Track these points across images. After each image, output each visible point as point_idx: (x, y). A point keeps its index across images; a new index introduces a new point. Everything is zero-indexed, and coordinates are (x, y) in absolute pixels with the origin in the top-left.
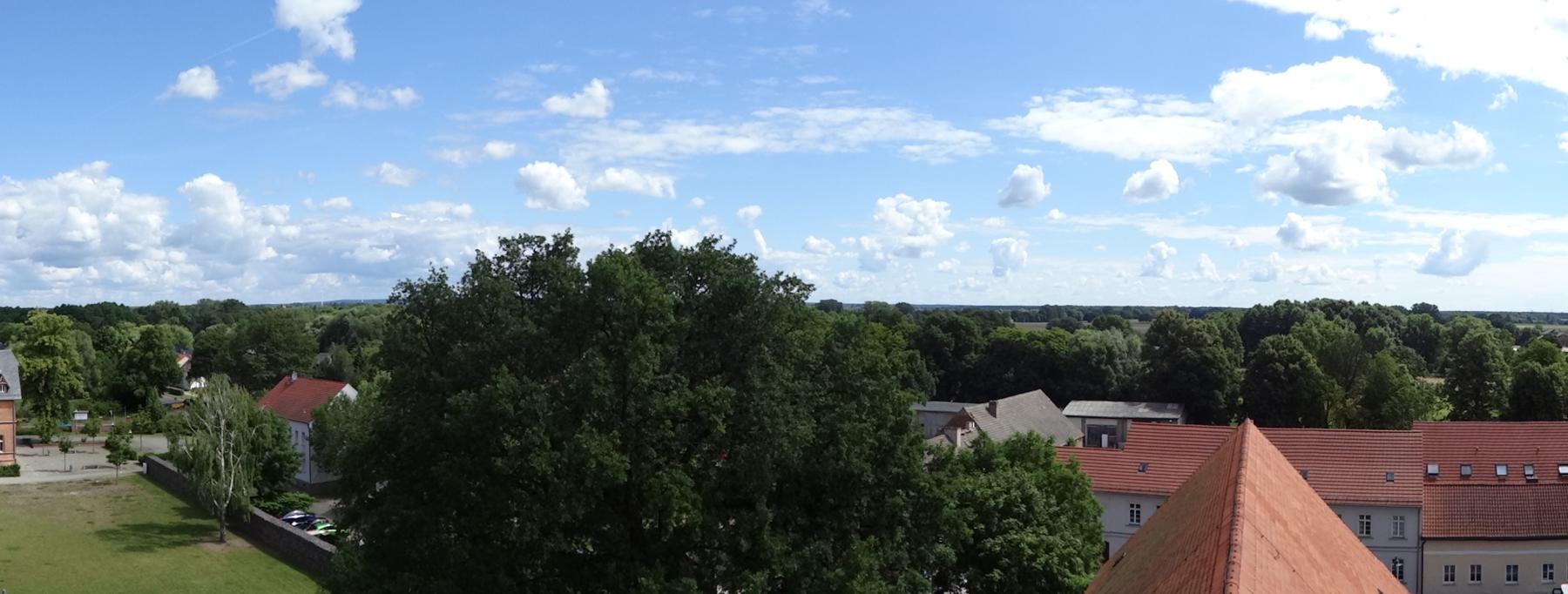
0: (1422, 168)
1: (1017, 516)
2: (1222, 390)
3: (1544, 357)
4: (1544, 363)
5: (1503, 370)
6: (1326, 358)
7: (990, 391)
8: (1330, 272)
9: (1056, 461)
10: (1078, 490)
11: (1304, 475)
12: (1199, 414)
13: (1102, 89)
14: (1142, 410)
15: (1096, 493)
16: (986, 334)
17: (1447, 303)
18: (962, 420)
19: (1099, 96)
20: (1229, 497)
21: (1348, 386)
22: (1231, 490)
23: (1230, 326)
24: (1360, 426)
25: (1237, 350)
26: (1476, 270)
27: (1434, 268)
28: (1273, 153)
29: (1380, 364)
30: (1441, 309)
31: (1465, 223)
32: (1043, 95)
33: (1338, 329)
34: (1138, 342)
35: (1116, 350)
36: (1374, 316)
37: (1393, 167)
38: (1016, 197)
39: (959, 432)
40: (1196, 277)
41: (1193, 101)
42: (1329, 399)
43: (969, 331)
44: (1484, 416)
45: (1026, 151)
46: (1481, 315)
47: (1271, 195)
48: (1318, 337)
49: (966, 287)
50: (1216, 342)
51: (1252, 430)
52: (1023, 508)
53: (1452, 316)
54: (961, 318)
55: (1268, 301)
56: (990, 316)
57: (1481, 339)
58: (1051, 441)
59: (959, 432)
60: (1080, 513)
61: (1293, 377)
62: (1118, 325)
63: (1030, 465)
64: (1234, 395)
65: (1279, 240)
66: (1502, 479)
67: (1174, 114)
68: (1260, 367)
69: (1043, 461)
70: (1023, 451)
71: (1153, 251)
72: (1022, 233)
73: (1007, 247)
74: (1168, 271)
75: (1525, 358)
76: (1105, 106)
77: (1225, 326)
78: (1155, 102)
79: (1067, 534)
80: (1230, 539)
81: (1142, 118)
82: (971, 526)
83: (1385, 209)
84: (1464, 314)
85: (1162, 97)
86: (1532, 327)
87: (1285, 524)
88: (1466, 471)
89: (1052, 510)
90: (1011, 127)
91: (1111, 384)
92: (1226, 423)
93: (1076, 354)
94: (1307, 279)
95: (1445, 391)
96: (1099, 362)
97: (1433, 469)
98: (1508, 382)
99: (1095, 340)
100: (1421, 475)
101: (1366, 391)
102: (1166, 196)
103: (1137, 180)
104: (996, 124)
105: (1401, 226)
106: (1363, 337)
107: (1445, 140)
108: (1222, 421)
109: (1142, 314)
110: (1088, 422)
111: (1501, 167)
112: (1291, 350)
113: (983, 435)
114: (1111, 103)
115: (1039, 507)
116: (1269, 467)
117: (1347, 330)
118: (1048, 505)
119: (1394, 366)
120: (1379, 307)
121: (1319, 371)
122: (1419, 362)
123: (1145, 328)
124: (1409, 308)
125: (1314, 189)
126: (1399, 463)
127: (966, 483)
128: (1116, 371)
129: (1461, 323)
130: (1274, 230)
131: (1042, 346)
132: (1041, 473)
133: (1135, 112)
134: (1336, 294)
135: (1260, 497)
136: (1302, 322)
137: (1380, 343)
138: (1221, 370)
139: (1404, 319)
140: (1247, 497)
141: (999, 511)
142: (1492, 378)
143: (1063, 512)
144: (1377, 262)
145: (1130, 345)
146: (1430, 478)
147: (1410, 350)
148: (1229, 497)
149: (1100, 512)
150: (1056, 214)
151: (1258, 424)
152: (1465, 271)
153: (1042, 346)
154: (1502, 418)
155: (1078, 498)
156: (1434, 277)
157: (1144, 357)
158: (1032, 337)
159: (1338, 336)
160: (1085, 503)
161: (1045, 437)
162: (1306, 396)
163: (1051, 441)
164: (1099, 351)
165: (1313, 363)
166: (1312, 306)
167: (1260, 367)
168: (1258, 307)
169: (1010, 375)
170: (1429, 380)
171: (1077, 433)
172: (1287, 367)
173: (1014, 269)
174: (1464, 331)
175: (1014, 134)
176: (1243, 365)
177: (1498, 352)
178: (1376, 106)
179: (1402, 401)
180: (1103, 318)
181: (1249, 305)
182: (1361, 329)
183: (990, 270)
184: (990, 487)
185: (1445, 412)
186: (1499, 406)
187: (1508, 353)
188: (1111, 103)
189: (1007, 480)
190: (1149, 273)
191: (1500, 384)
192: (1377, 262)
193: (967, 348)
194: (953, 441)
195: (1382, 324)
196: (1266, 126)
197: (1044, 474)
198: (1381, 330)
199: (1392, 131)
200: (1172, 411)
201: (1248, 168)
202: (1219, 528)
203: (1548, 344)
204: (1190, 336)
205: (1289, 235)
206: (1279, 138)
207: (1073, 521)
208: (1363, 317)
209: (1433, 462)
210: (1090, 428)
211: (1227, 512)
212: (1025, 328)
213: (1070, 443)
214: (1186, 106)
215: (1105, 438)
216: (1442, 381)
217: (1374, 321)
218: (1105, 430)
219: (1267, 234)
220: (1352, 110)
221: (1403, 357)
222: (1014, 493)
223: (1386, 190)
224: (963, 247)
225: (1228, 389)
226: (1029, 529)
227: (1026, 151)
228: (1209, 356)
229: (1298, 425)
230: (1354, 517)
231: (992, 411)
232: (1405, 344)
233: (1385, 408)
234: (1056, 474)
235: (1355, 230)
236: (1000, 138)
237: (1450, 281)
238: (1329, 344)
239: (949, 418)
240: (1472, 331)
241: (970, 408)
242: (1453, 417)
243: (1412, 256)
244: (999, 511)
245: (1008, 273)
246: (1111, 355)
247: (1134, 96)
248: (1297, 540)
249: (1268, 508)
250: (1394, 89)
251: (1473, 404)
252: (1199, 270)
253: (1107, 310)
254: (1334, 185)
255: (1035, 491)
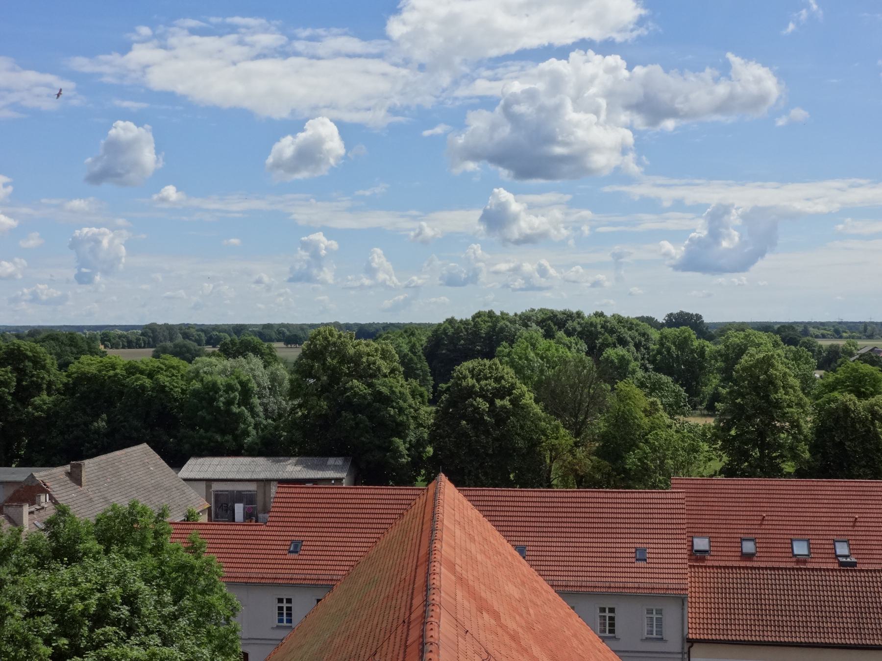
0: (684, 122)
1: (116, 622)
2: (403, 437)
3: (860, 386)
4: (861, 395)
5: (800, 405)
6: (548, 393)
7: (70, 445)
8: (552, 272)
9: (169, 543)
10: (202, 582)
11: (521, 550)
12: (373, 470)
13: (237, 20)
14: (292, 469)
15: (233, 584)
16: (64, 366)
17: (713, 314)
18: (29, 493)
19: (233, 29)
20: (420, 581)
21: (577, 430)
22: (421, 572)
23: (413, 348)
24: (597, 485)
25: (423, 383)
26: (760, 264)
27: (696, 262)
28: (474, 107)
29: (623, 398)
30: (707, 319)
31: (742, 197)
32: (152, 25)
33: (562, 350)
34: (285, 375)
35: (253, 385)
36: (612, 331)
37: (639, 121)
38: (110, 170)
39: (26, 509)
40: (367, 282)
41: (364, 37)
42: (553, 448)
43: (37, 363)
44: (774, 471)
45: (127, 104)
46: (766, 328)
47: (471, 166)
48: (537, 363)
49: (35, 299)
50: (393, 371)
51: (447, 488)
52: (125, 611)
53: (724, 329)
54: (26, 345)
55: (464, 313)
56: (69, 342)
57: (767, 363)
58: (162, 515)
59: (26, 509)
60: (207, 612)
61: (500, 416)
62: (256, 351)
63: (133, 549)
64: (419, 444)
65: (482, 228)
66: (800, 560)
67: (337, 54)
68: (455, 405)
69: (151, 543)
70: (120, 531)
71: (305, 246)
72: (120, 222)
73: (96, 241)
74: (328, 275)
75: (832, 387)
76: (241, 43)
77: (406, 349)
78: (312, 39)
79: (188, 643)
80: (422, 636)
81: (293, 61)
82: (48, 641)
83: (629, 180)
84: (741, 327)
85: (321, 31)
86: (841, 343)
87: (496, 615)
88: (749, 547)
89: (166, 611)
90: (105, 69)
91: (246, 433)
92: (410, 481)
93: (196, 393)
94: (519, 283)
95: (719, 434)
96: (229, 403)
97: (701, 544)
98: (808, 423)
99: (223, 372)
100: (684, 554)
101: (603, 437)
102: (324, 170)
103: (287, 146)
104: (82, 64)
105: (651, 206)
106: (597, 362)
107: (716, 80)
108: (404, 478)
109: (289, 335)
110: (216, 487)
111: (799, 113)
112: (498, 380)
113: (63, 511)
114: (248, 39)
115: (148, 607)
116: (472, 539)
117: (573, 351)
118: (160, 603)
119: (641, 400)
120: (620, 320)
121: (537, 409)
122: (677, 395)
123: (292, 353)
124: (661, 318)
125: (532, 156)
126: (656, 536)
127: (39, 582)
128: (254, 414)
129: (736, 339)
130: (476, 214)
131: (147, 382)
132: (150, 560)
133: (283, 53)
134: (557, 301)
135: (461, 579)
136: (512, 341)
137: (621, 370)
138: (401, 410)
139: (655, 335)
140: (443, 578)
141: (90, 617)
142: (784, 417)
143: (182, 613)
144: (618, 256)
145: (273, 378)
146: (697, 556)
147: (665, 378)
148: (420, 581)
149: (234, 610)
150: (170, 192)
151: (458, 482)
152: (743, 266)
153: (147, 382)
154: (800, 474)
155: (203, 592)
156: (697, 276)
157: (293, 393)
158: (132, 370)
159: (565, 362)
160: (213, 599)
161: (153, 508)
162: (520, 444)
163: (162, 515)
164: (229, 388)
165: (529, 399)
166: (525, 320)
167: (455, 405)
168: (451, 321)
169: (101, 424)
170: (693, 421)
171: (199, 502)
172: (492, 403)
173: (106, 273)
174: (741, 351)
175: (107, 80)
176: (432, 402)
177: (792, 380)
178: (619, 38)
179: (654, 450)
180: (237, 342)
181: (437, 318)
182: (594, 351)
183: (71, 274)
184: (76, 584)
185: (717, 465)
186: (795, 457)
187: (806, 381)
188: (248, 39)
189: (101, 572)
190: (300, 277)
191: (795, 425)
192: (618, 256)
193: (37, 388)
194: (15, 522)
195: (622, 342)
196: (465, 69)
197: (154, 562)
198: (621, 351)
199: (639, 70)
200: (335, 468)
201: (439, 130)
202: (407, 623)
203: (867, 368)
204: (357, 363)
205: (496, 220)
206: (483, 87)
207: (198, 625)
208: (596, 334)
209: (702, 534)
210: (218, 496)
211: (418, 600)
212: (122, 357)
213: (190, 518)
214: (354, 44)
215: (239, 508)
216: (711, 421)
217: (611, 339)
218: (239, 497)
219: (469, 219)
220: (584, 45)
221: (655, 388)
222: (113, 590)
223: (631, 156)
224: (33, 241)
225: (412, 437)
226: (134, 640)
227: (127, 104)
228: (385, 390)
229: (509, 484)
230: (593, 608)
231: (75, 477)
232: (657, 369)
233: (632, 460)
234: (171, 560)
235: (586, 213)
236: (87, 83)
237: (722, 279)
238: (550, 373)
239: (11, 491)
240: (752, 350)
241: (41, 474)
242: (729, 472)
243: (667, 246)
244: (90, 617)
245: (98, 278)
246: (246, 392)
247: (282, 30)
248: (514, 638)
249: (472, 594)
250: (643, 12)
251: (756, 453)
252: (371, 271)
253: (239, 329)
254: (558, 150)
255: (142, 585)
